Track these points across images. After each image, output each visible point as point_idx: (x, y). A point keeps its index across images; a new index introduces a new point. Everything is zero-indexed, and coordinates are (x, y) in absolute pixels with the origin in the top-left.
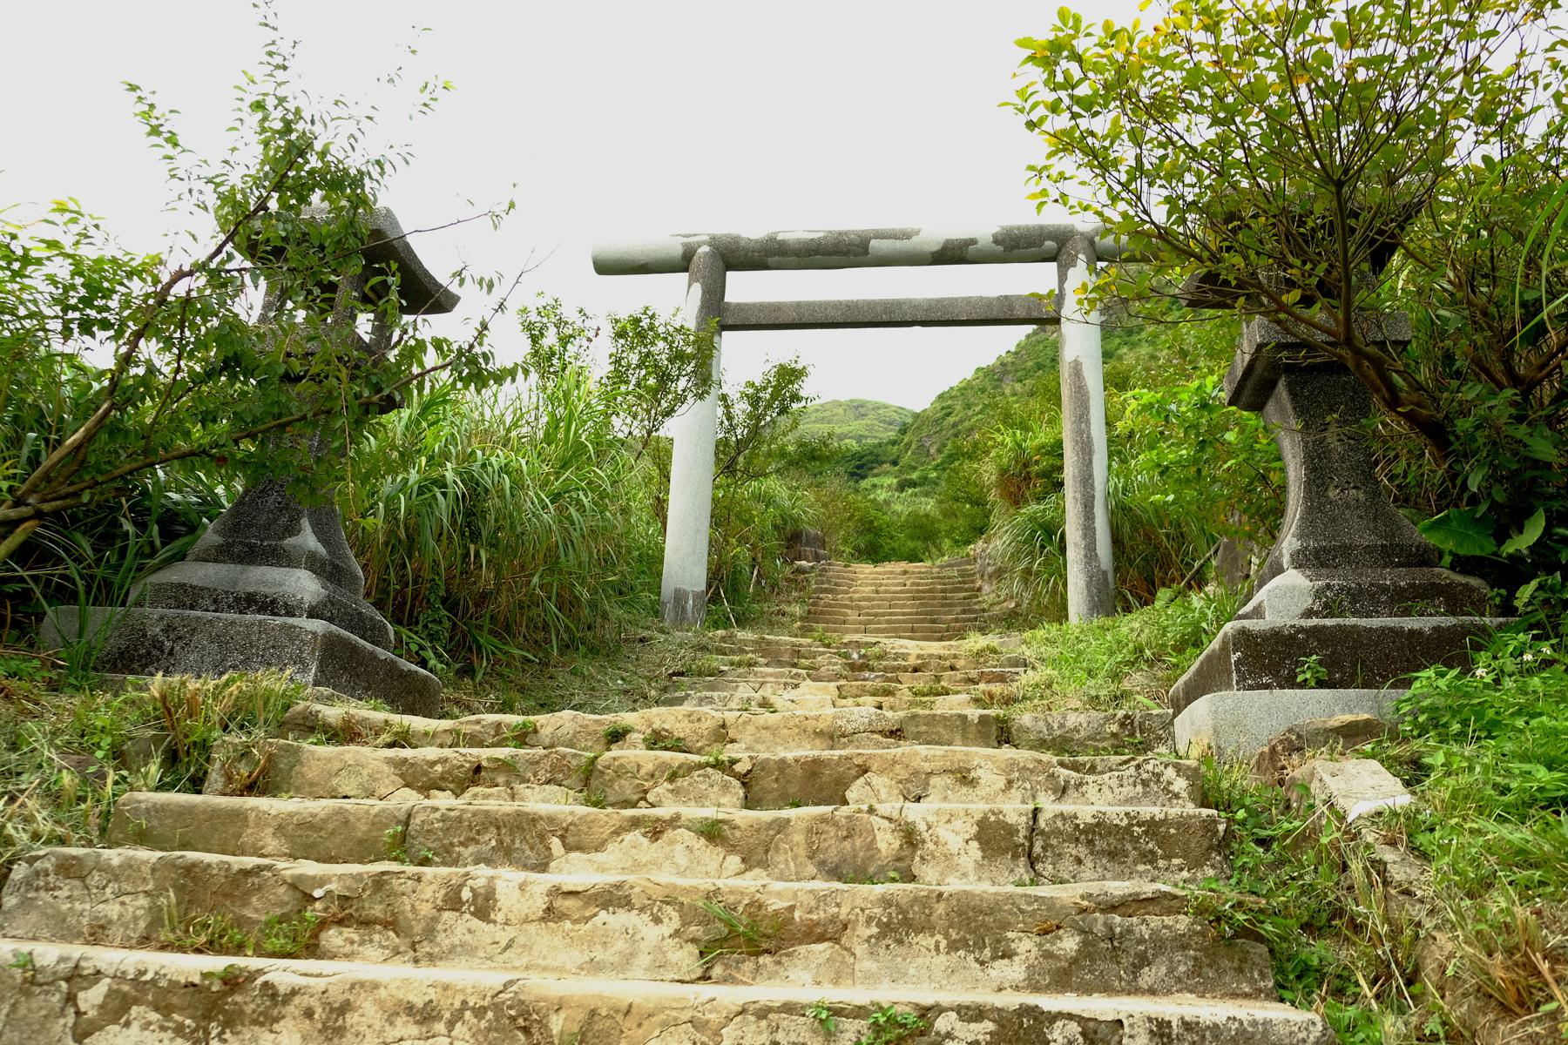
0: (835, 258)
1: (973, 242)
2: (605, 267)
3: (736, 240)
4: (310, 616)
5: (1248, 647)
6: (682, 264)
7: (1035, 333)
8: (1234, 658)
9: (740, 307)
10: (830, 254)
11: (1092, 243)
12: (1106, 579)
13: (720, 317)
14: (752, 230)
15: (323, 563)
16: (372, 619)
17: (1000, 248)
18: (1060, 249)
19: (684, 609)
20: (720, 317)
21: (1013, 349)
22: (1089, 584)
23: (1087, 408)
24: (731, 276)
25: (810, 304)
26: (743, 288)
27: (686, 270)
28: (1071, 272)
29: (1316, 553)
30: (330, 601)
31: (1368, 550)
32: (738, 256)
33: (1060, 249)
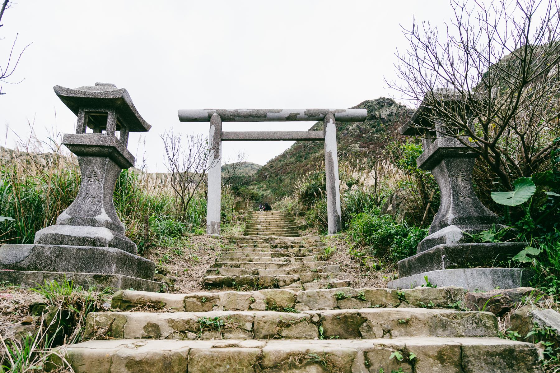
0: (256, 118)
1: (299, 114)
2: (183, 119)
3: (225, 110)
4: (110, 246)
5: (447, 253)
6: (208, 119)
7: (296, 143)
8: (443, 257)
9: (228, 133)
10: (255, 117)
11: (334, 115)
12: (339, 218)
13: (220, 137)
14: (230, 107)
15: (111, 224)
16: (130, 243)
17: (306, 116)
18: (324, 117)
19: (214, 227)
20: (220, 137)
21: (290, 148)
22: (334, 219)
23: (333, 166)
24: (224, 123)
25: (288, 132)
26: (228, 127)
27: (209, 121)
28: (328, 124)
29: (460, 219)
30: (116, 239)
31: (477, 218)
32: (226, 117)
33: (324, 117)
